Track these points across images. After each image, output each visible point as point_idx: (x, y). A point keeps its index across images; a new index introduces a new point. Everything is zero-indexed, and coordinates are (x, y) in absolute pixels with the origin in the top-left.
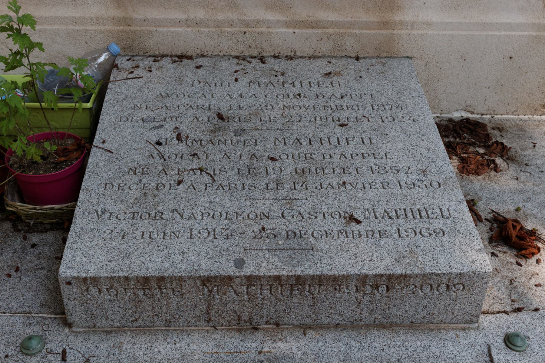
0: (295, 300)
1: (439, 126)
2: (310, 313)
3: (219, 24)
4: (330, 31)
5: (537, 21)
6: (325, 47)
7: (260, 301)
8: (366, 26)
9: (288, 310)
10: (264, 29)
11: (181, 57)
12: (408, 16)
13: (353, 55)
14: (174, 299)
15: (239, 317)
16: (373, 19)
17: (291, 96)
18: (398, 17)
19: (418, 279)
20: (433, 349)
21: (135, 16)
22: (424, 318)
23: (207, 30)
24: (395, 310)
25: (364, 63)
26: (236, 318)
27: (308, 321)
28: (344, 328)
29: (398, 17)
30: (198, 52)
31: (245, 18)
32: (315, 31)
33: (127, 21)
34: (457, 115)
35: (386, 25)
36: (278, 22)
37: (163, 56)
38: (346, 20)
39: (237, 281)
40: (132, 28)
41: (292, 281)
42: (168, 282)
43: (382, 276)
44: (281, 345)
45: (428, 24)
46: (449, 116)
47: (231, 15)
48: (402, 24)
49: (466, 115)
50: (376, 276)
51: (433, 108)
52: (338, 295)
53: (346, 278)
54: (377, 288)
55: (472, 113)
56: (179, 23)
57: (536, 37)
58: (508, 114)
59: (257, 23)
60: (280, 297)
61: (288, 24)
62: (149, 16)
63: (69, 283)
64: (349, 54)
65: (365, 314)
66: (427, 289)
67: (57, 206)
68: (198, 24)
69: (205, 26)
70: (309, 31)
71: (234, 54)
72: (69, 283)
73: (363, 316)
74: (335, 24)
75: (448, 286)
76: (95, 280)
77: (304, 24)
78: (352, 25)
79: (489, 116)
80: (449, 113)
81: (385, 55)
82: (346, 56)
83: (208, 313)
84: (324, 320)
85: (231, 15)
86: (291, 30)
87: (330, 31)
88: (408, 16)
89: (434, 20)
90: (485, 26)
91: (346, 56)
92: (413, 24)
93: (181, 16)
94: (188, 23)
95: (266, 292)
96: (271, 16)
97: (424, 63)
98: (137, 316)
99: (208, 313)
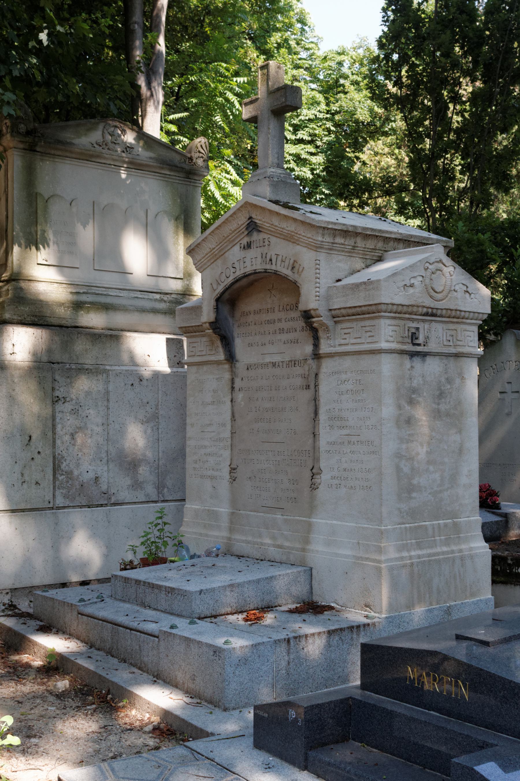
18: (308, 547)
56: (243, 541)
61: (275, 546)
74: (288, 547)
93: (244, 538)
94: (248, 542)
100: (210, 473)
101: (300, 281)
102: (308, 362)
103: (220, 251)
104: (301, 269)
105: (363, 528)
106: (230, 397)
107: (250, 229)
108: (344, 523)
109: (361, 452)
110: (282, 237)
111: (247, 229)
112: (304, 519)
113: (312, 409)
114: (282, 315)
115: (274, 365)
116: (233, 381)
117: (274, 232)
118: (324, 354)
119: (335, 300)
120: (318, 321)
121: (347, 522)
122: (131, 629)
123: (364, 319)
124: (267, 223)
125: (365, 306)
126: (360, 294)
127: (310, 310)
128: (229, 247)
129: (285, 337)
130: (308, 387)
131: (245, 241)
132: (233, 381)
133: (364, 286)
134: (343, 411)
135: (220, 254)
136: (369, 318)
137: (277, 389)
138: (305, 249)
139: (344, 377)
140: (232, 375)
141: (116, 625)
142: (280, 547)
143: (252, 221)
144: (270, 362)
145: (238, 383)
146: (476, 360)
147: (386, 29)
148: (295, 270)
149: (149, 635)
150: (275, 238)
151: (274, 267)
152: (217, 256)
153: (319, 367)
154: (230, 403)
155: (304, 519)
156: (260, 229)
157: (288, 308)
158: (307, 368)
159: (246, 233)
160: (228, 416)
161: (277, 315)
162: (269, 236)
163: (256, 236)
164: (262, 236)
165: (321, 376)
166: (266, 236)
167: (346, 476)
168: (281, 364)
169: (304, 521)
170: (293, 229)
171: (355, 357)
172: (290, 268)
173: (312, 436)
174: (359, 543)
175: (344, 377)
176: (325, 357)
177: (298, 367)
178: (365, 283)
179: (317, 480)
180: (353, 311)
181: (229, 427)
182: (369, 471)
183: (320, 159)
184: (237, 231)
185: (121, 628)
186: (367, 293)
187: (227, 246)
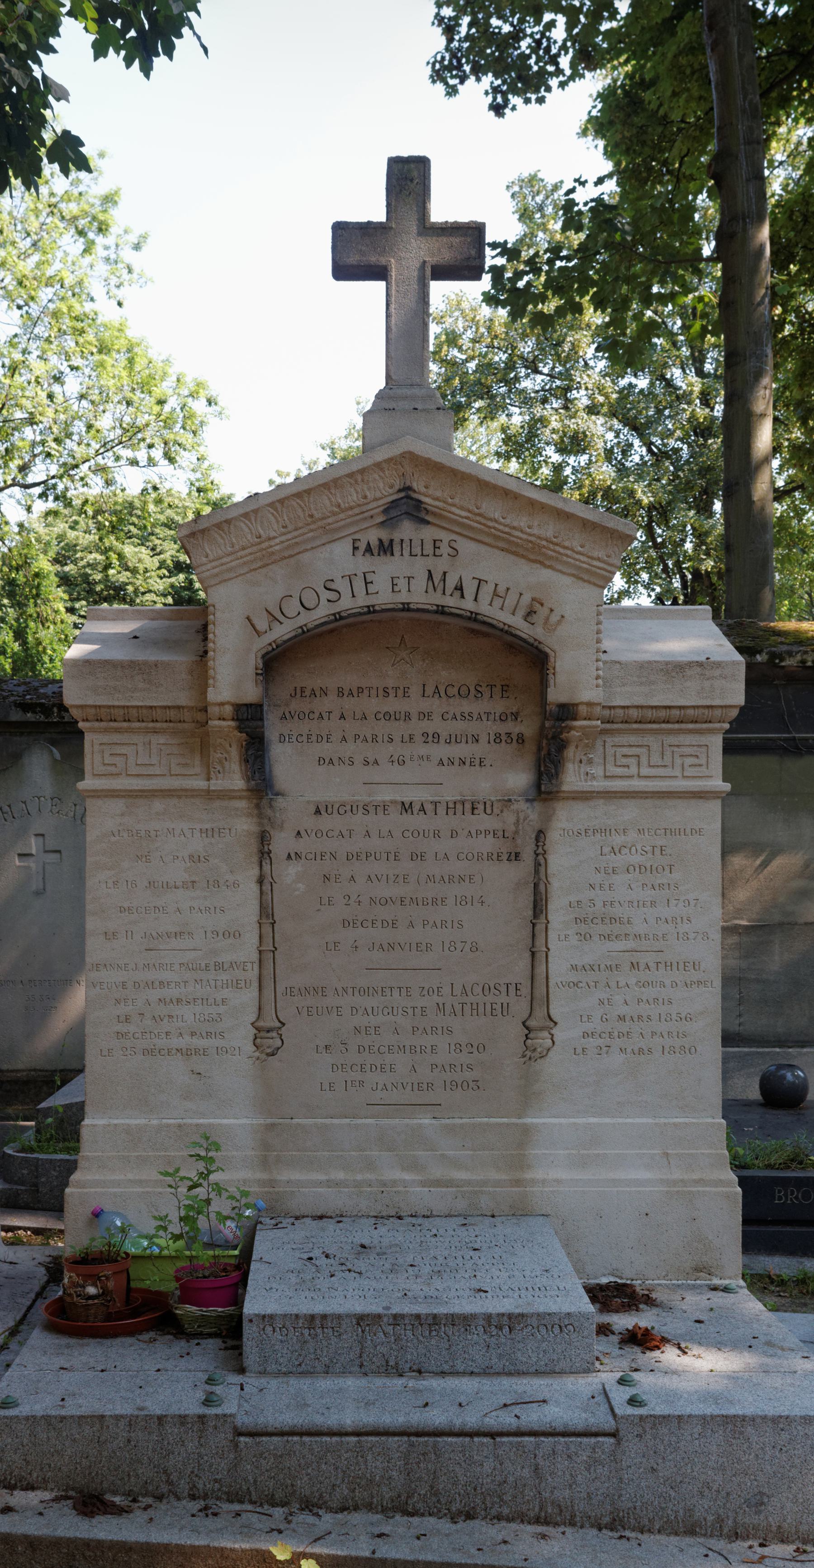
0: (433, 1342)
1: (584, 1287)
2: (447, 1358)
3: (358, 1184)
4: (465, 1189)
5: (664, 1177)
6: (461, 1205)
7: (403, 1343)
8: (498, 1183)
9: (428, 1355)
10: (401, 1189)
11: (321, 1217)
12: (539, 1174)
13: (490, 1214)
14: (334, 1340)
15: (387, 1362)
16: (504, 1177)
17: (397, 739)
18: (529, 1175)
19: (534, 1319)
20: (555, 1386)
21: (279, 1177)
22: (546, 1365)
23: (346, 1190)
24: (519, 1354)
25: (498, 1220)
26: (384, 1364)
27: (446, 1368)
28: (478, 1374)
29: (529, 1175)
30: (338, 1212)
31: (383, 1178)
32: (450, 1189)
33: (272, 1183)
34: (604, 1280)
35: (518, 1183)
36: (414, 1181)
37: (303, 1217)
38: (479, 1178)
39: (385, 1319)
40: (276, 1190)
41: (430, 1321)
42: (329, 1319)
43: (503, 1315)
44: (424, 1383)
45: (558, 1181)
46: (597, 1281)
47: (369, 1176)
48: (533, 1182)
49: (612, 1279)
50: (498, 1315)
51: (579, 1271)
52: (469, 1337)
53: (474, 1316)
54: (501, 1329)
55: (621, 1278)
56: (320, 1184)
57: (667, 1192)
58: (659, 1279)
59: (394, 1183)
60: (421, 1338)
61: (423, 1184)
62: (293, 1178)
63: (251, 1321)
64: (484, 1213)
65: (495, 1360)
66: (543, 1331)
67: (220, 1309)
68: (337, 1184)
69: (347, 1186)
70: (444, 1189)
71: (372, 1214)
72: (251, 1321)
73: (493, 1362)
74: (469, 1183)
75: (560, 1327)
76: (271, 1317)
77: (438, 1183)
78: (485, 1183)
79: (639, 1282)
80: (596, 1278)
81: (520, 1212)
82: (482, 1215)
83: (361, 1357)
84: (460, 1367)
85: (369, 1176)
86: (426, 1189)
87: (465, 1189)
88: (539, 1174)
89: (564, 1177)
90: (615, 1182)
91: (482, 1215)
92: (544, 1182)
93: (322, 1177)
94: (329, 1183)
95: (409, 1333)
96: (407, 1176)
97: (560, 1222)
98: (301, 1359)
99: (361, 1357)
100: (186, 1041)
101: (550, 642)
102: (515, 807)
103: (287, 548)
104: (554, 618)
105: (675, 1124)
106: (256, 871)
107: (394, 513)
108: (620, 1120)
109: (668, 983)
110: (501, 544)
111: (385, 511)
112: (505, 1120)
113: (526, 899)
114: (435, 705)
115: (406, 808)
116: (263, 838)
117: (480, 531)
118: (569, 792)
119: (618, 689)
120: (583, 728)
121: (628, 1117)
122: (493, 1435)
123: (671, 732)
124: (462, 508)
125: (694, 707)
126: (688, 684)
127: (577, 705)
128: (318, 543)
129: (442, 751)
130: (517, 856)
131: (373, 536)
132: (263, 838)
133: (699, 669)
134: (617, 904)
135: (286, 554)
136: (691, 731)
137: (417, 857)
138: (567, 580)
139: (618, 840)
140: (260, 824)
141: (418, 1434)
142: (438, 1183)
143: (408, 497)
144: (393, 802)
145: (281, 843)
146: (719, 802)
147: (601, 143)
148: (539, 618)
149: (564, 1434)
150: (473, 546)
151: (468, 604)
152: (276, 557)
153: (547, 818)
154: (255, 888)
155: (505, 1120)
156: (429, 518)
157: (453, 691)
158: (510, 818)
159: (381, 519)
160: (250, 913)
161: (415, 704)
162: (454, 537)
163: (407, 530)
164: (428, 533)
165: (554, 836)
166: (445, 536)
167: (625, 1030)
168: (429, 807)
169: (508, 1125)
170: (550, 534)
171: (649, 803)
172: (521, 612)
173: (528, 955)
174: (667, 1155)
175: (618, 840)
176: (568, 798)
177: (483, 815)
178: (700, 664)
179: (542, 1040)
180: (662, 714)
181: (251, 939)
182: (689, 1018)
183: (615, 396)
184: (357, 511)
185: (527, 1439)
186: (707, 684)
187: (314, 538)
